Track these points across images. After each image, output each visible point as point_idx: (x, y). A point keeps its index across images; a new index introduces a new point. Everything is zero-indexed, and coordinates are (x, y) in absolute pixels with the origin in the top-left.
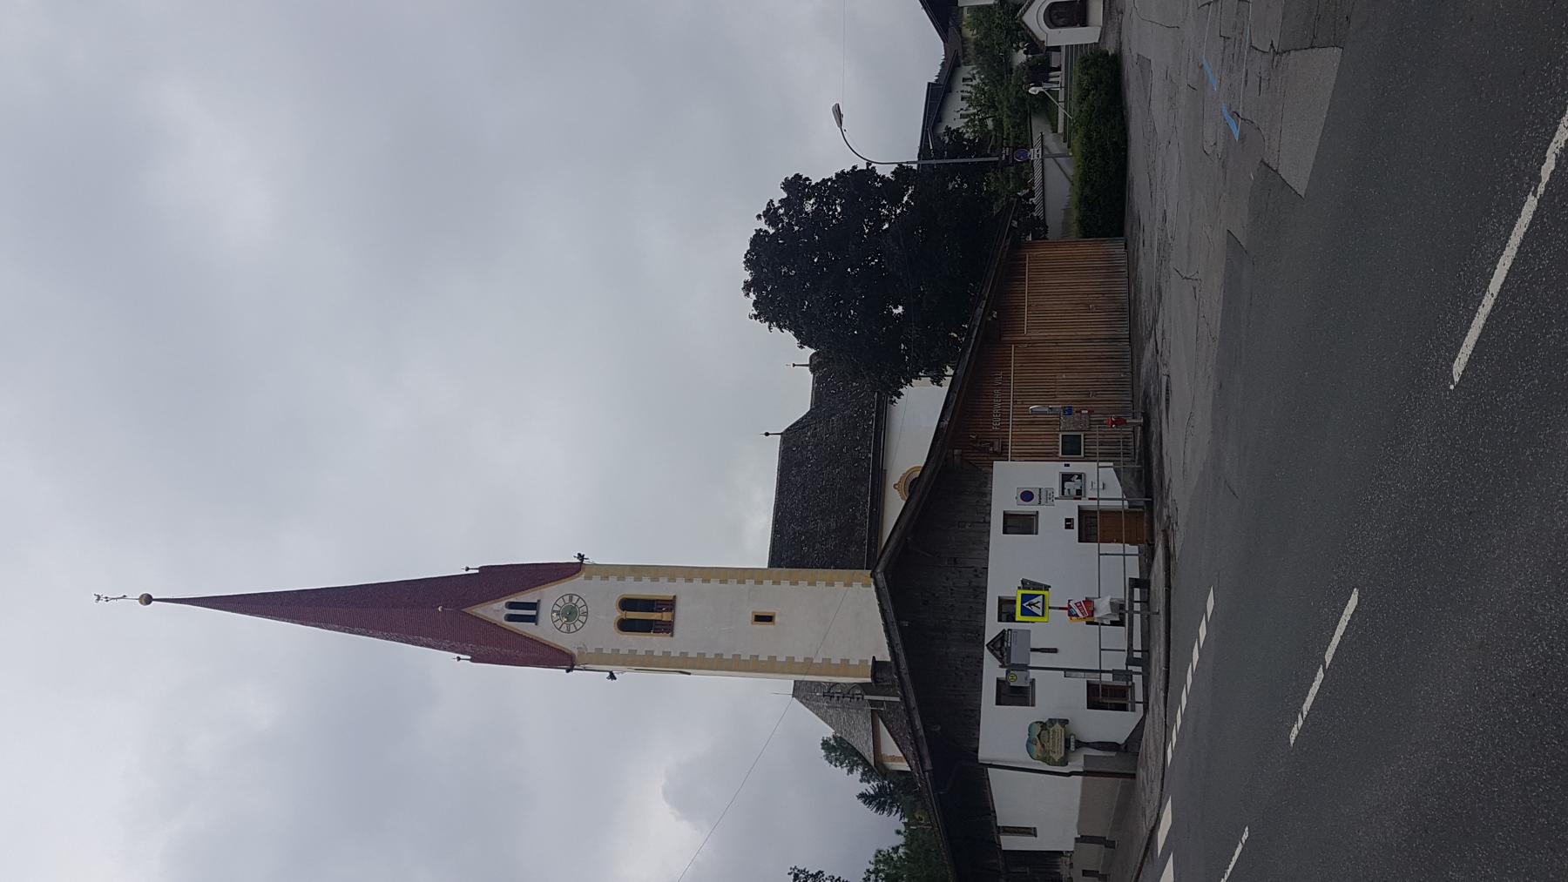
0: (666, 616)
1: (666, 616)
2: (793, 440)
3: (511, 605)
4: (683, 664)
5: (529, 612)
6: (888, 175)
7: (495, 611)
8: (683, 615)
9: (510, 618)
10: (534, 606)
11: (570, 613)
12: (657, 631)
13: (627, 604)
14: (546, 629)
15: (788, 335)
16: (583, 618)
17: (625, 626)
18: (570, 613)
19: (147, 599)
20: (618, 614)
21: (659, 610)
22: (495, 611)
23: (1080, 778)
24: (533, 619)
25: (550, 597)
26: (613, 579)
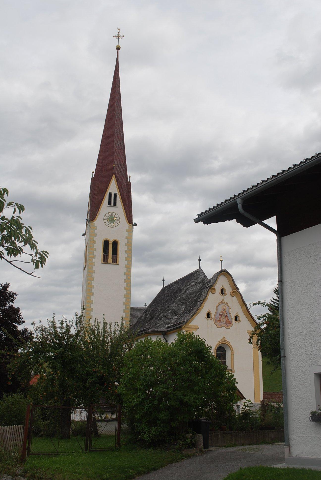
0: (110, 260)
1: (110, 260)
2: (93, 180)
3: (115, 195)
4: (88, 265)
5: (112, 202)
6: (72, 419)
7: (113, 188)
8: (109, 268)
9: (110, 195)
10: (115, 204)
11: (112, 220)
12: (104, 256)
13: (115, 244)
14: (105, 209)
15: (242, 225)
16: (106, 217)
17: (106, 243)
18: (112, 220)
19: (118, 49)
20: (111, 240)
21: (112, 258)
22: (113, 188)
23: (115, 422)
24: (110, 203)
25: (119, 210)
26: (126, 234)
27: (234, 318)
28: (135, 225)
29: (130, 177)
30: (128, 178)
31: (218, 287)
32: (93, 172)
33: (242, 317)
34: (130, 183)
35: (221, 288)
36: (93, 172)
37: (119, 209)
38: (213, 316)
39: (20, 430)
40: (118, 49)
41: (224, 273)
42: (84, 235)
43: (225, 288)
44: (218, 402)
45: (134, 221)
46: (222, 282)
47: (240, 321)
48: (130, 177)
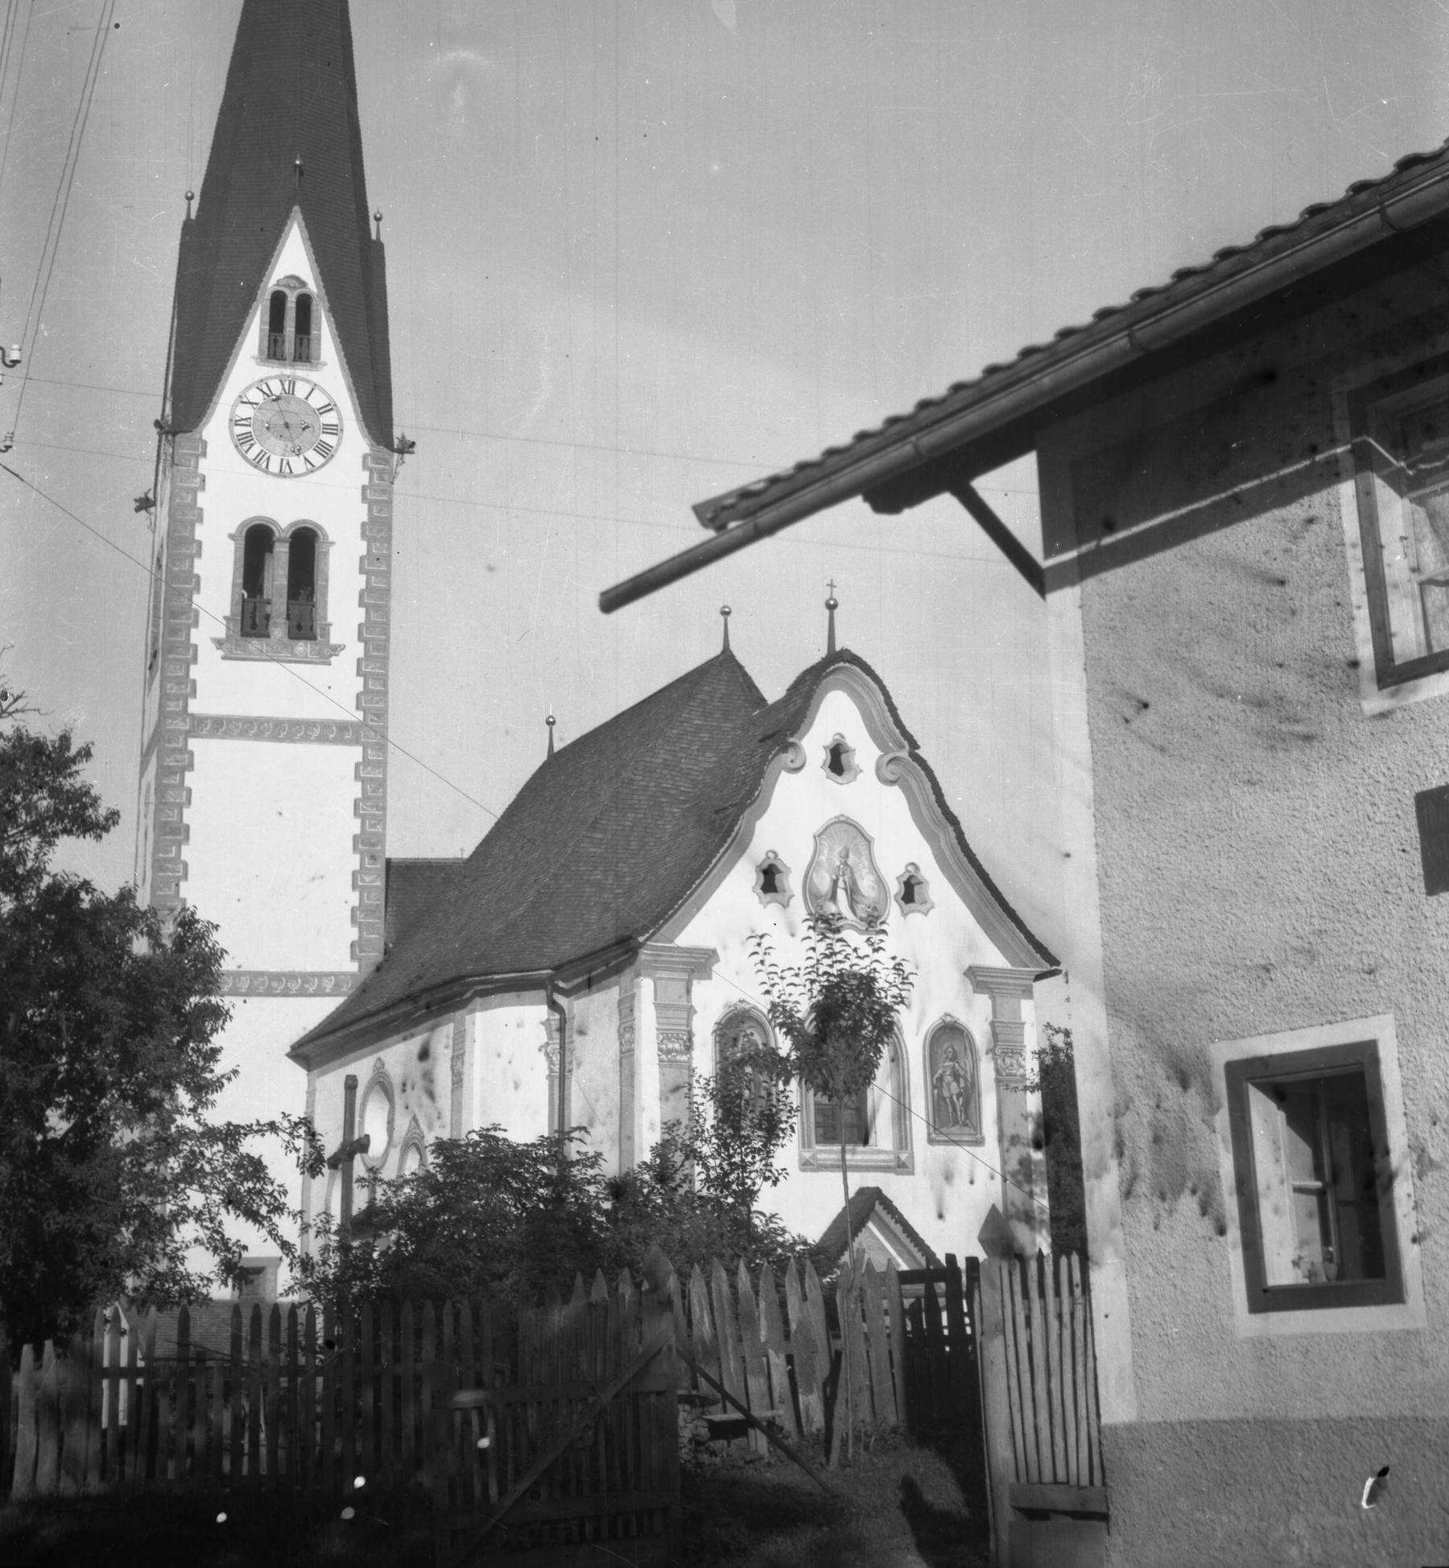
2: (188, 226)
3: (304, 303)
7: (294, 260)
9: (278, 300)
14: (248, 369)
19: (832, 607)
22: (294, 260)
27: (895, 888)
28: (407, 447)
29: (378, 219)
30: (373, 223)
31: (813, 744)
32: (190, 199)
33: (938, 886)
34: (379, 247)
35: (829, 741)
36: (190, 199)
37: (328, 378)
38: (793, 882)
39: (1043, 1415)
40: (832, 607)
41: (837, 664)
42: (145, 504)
43: (850, 742)
44: (178, 1178)
45: (400, 428)
46: (837, 715)
47: (927, 907)
48: (378, 219)
